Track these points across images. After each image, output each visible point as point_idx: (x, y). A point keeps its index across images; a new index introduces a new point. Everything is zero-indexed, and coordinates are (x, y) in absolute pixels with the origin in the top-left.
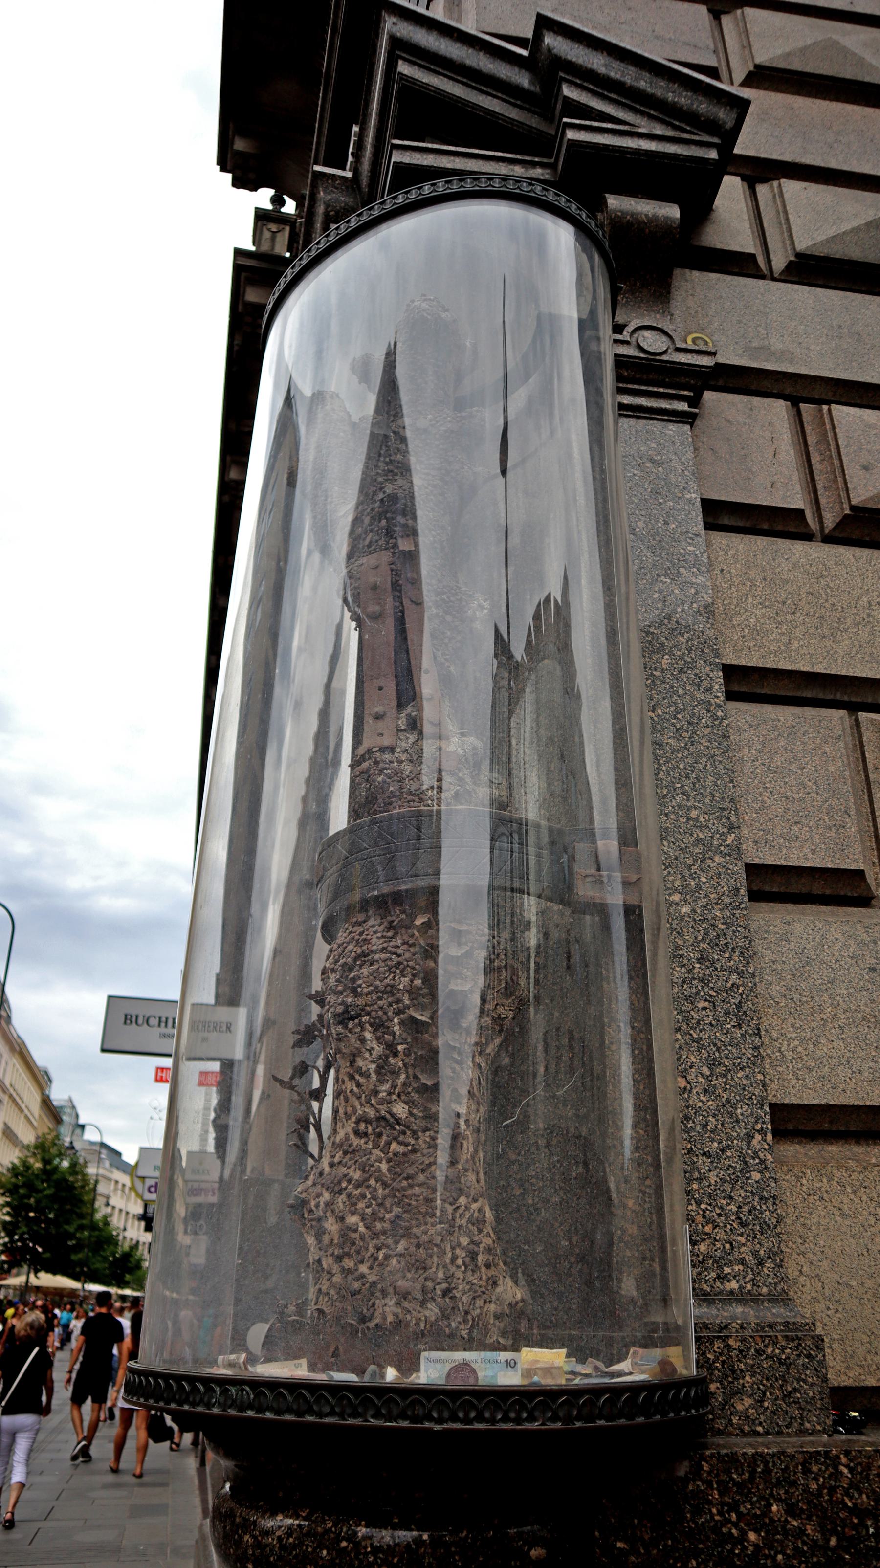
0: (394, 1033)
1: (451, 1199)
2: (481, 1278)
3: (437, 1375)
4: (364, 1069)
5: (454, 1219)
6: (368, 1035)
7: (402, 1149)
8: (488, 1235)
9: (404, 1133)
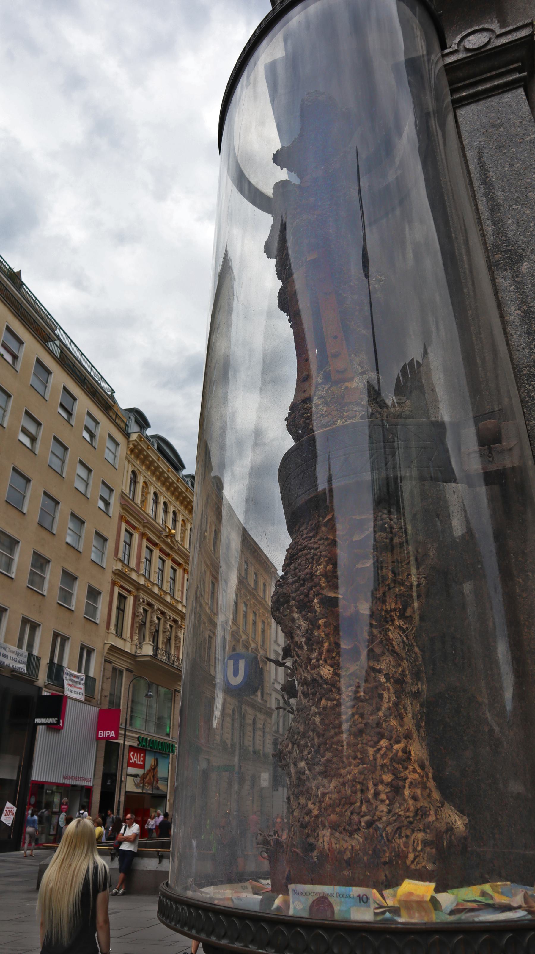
0: (315, 612)
1: (372, 743)
2: (408, 810)
3: (301, 907)
4: (299, 643)
5: (375, 759)
6: (296, 616)
7: (329, 704)
8: (414, 771)
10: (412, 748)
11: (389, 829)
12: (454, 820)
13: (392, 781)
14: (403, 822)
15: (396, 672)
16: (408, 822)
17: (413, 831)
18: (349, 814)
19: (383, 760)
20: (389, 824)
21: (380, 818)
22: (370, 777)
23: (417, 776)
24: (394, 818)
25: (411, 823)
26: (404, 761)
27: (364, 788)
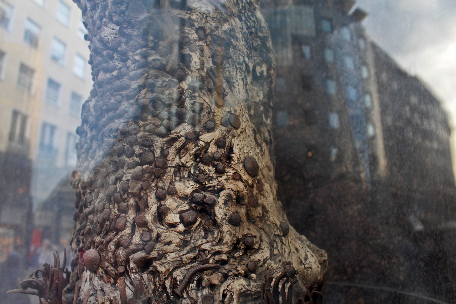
5: (164, 155)
8: (237, 177)
9: (112, 58)
10: (235, 141)
11: (179, 274)
12: (303, 255)
13: (194, 192)
14: (207, 261)
15: (217, 28)
16: (217, 262)
17: (225, 277)
18: (113, 247)
19: (180, 158)
20: (180, 264)
21: (162, 255)
22: (153, 185)
23: (241, 185)
24: (191, 255)
25: (224, 263)
26: (220, 160)
27: (141, 205)
